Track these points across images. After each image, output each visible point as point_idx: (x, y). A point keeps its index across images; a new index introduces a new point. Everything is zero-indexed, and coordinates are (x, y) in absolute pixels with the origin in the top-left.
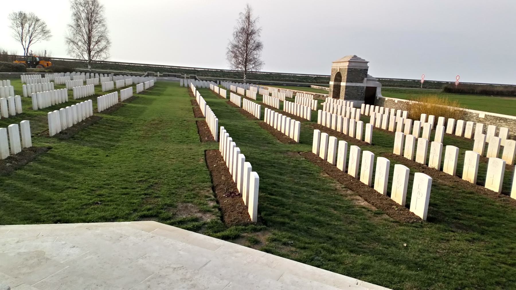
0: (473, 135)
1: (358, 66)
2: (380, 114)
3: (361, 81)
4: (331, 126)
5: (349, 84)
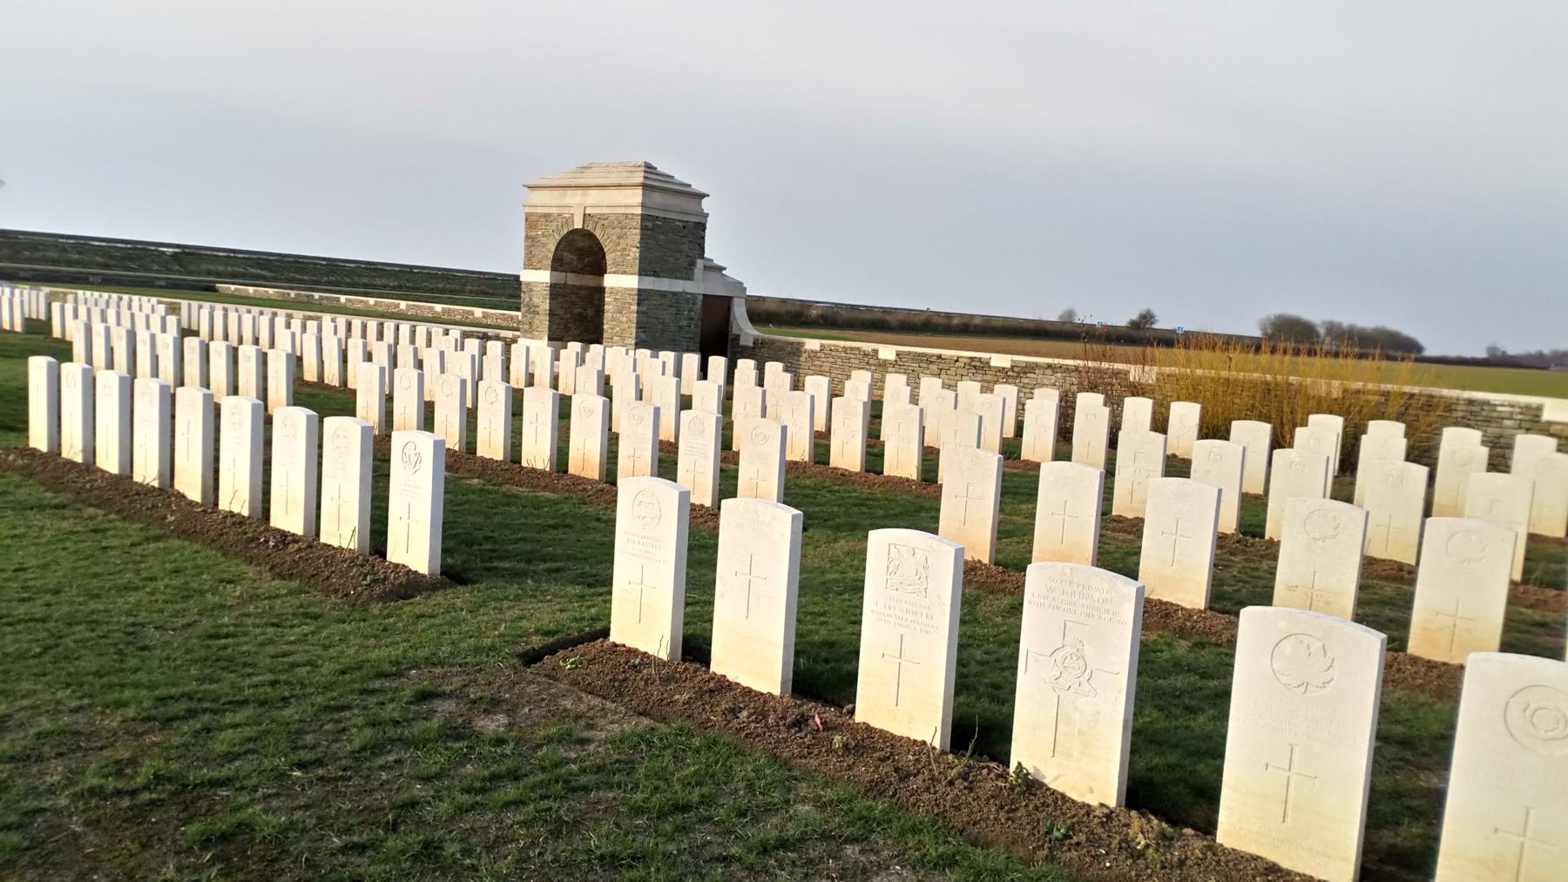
0: (929, 458)
1: (674, 208)
2: (373, 370)
3: (686, 273)
4: (90, 450)
5: (652, 283)
